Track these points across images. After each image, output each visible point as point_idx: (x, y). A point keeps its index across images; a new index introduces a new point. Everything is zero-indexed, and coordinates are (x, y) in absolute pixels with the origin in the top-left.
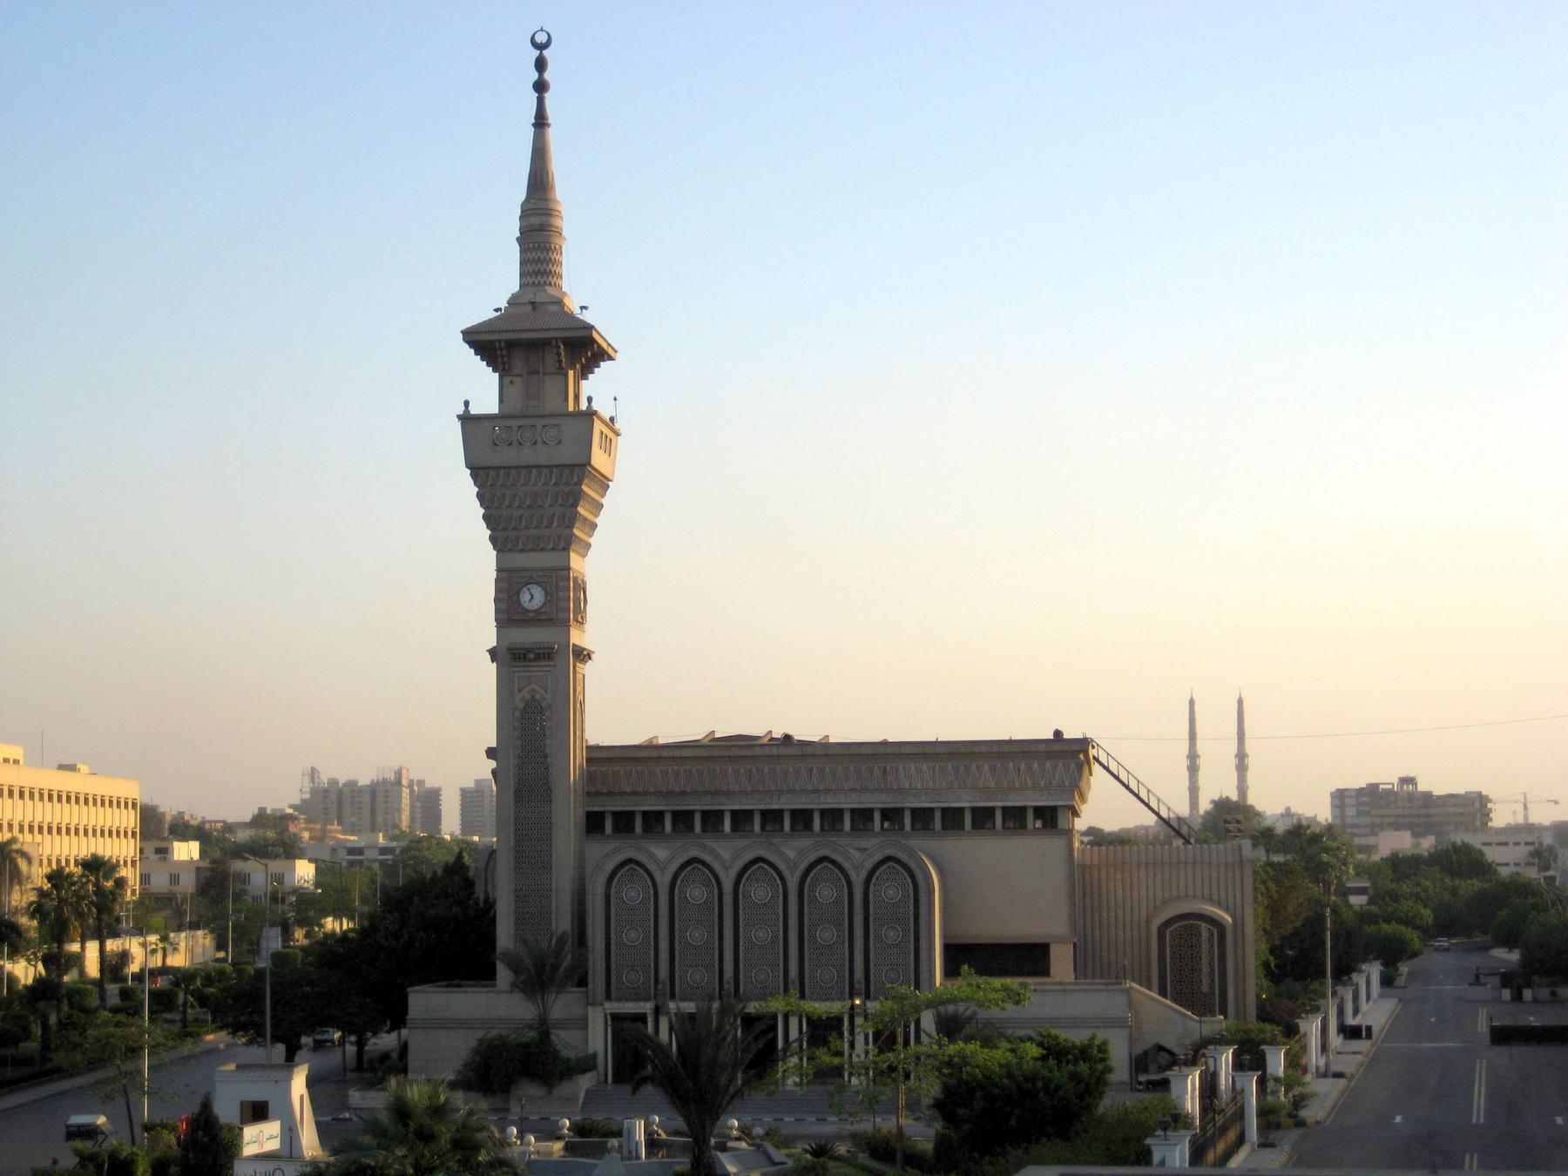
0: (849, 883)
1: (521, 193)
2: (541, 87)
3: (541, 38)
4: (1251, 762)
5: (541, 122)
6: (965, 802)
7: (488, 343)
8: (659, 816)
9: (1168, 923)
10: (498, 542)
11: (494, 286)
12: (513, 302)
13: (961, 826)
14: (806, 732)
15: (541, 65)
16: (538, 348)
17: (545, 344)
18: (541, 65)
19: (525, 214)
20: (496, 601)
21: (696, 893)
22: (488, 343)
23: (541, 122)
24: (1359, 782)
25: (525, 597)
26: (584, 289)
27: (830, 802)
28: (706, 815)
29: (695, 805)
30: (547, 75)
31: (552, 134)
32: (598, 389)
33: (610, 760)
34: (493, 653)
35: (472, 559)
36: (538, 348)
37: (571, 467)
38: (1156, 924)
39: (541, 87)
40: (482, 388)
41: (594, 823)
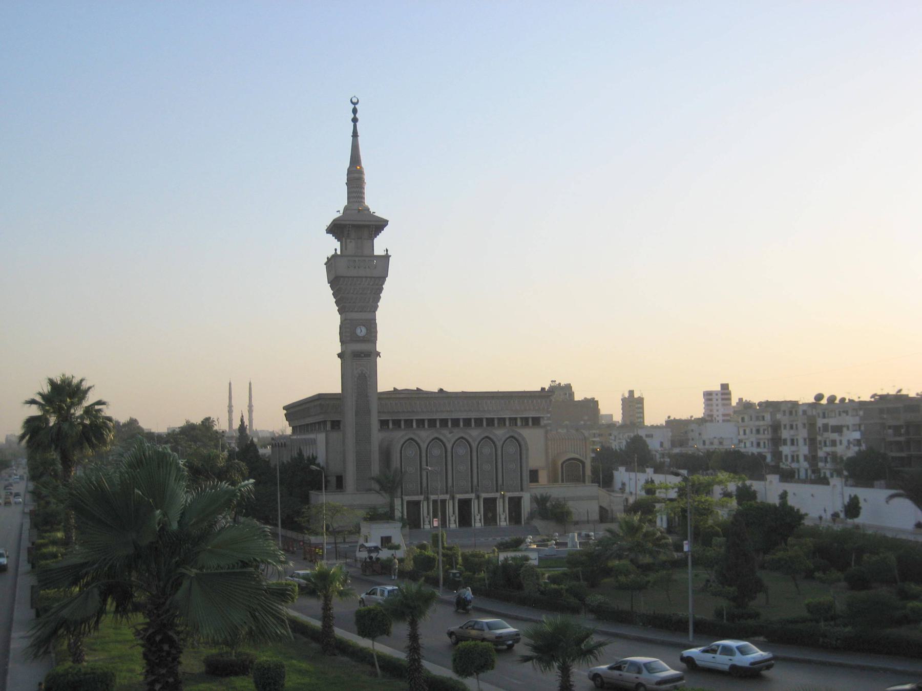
0: (495, 446)
1: (347, 164)
2: (355, 120)
3: (355, 100)
4: (255, 409)
5: (355, 135)
6: (507, 415)
7: (336, 229)
8: (492, 420)
9: (564, 462)
10: (340, 311)
11: (336, 204)
12: (346, 209)
13: (493, 425)
14: (451, 387)
15: (355, 111)
16: (356, 228)
17: (368, 226)
18: (355, 111)
19: (350, 172)
20: (376, 332)
21: (436, 452)
22: (336, 229)
23: (355, 135)
24: (763, 400)
25: (358, 331)
26: (375, 202)
27: (455, 416)
28: (406, 421)
29: (402, 417)
30: (357, 116)
31: (360, 139)
32: (380, 245)
33: (330, 399)
34: (339, 355)
35: (327, 318)
36: (356, 228)
37: (379, 278)
38: (560, 463)
39: (355, 120)
40: (332, 245)
41: (384, 424)
